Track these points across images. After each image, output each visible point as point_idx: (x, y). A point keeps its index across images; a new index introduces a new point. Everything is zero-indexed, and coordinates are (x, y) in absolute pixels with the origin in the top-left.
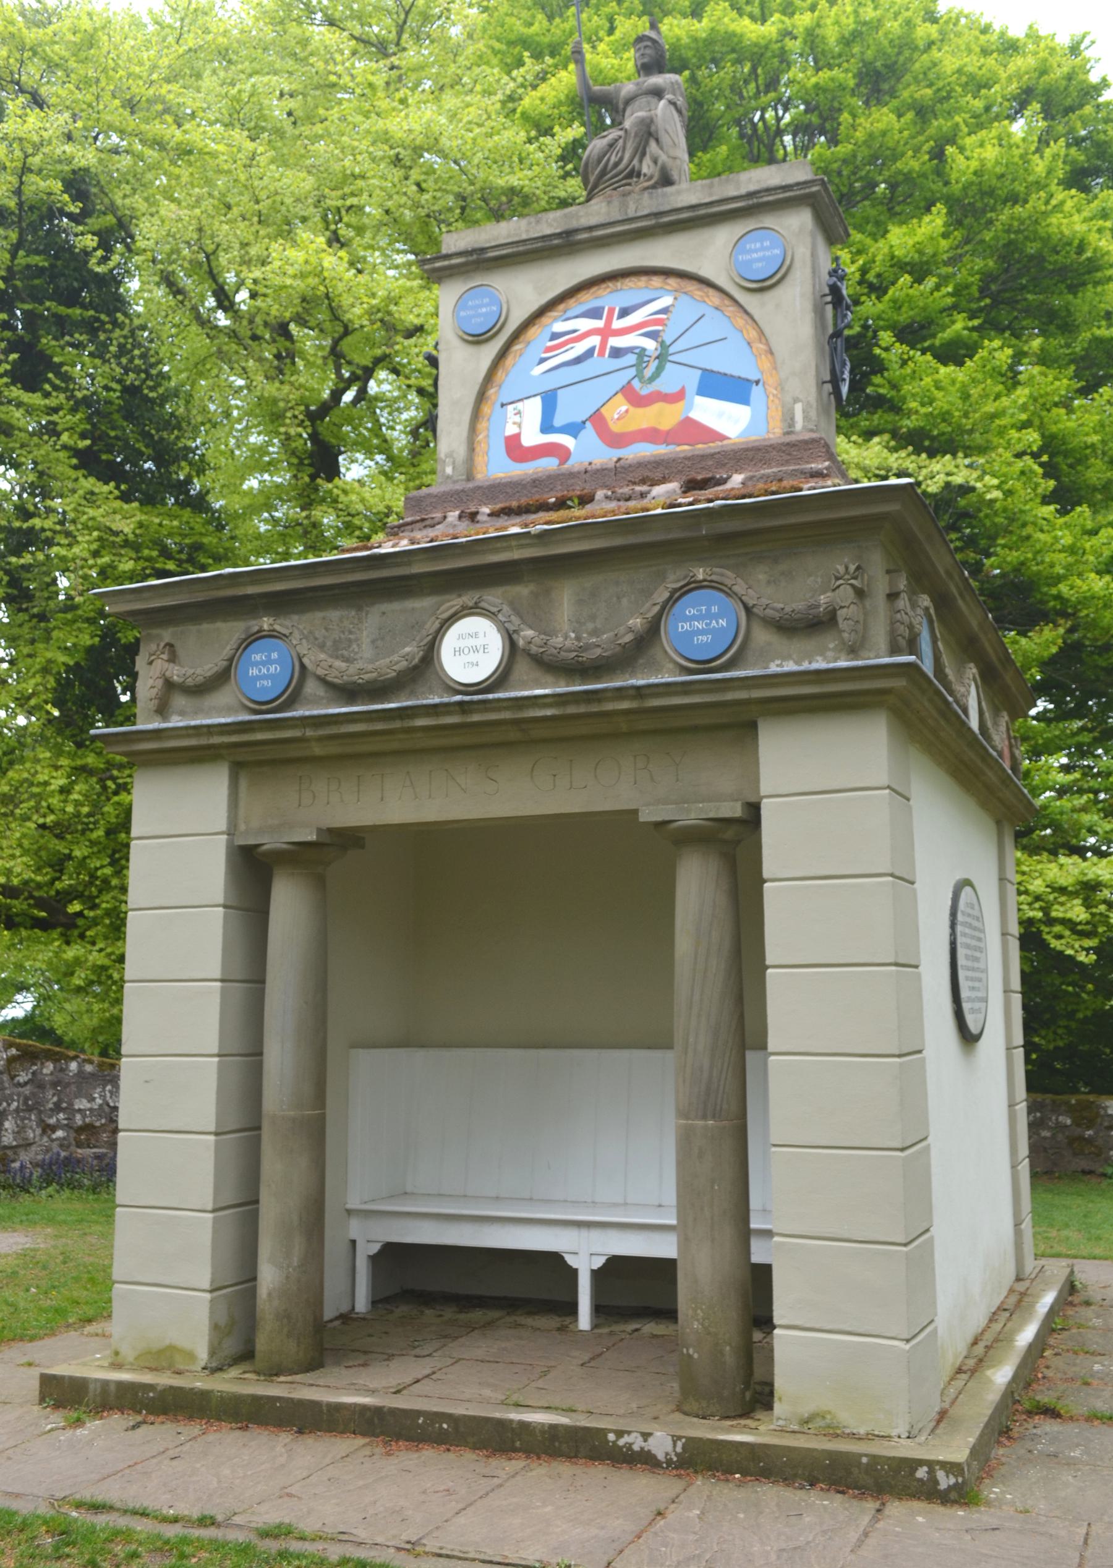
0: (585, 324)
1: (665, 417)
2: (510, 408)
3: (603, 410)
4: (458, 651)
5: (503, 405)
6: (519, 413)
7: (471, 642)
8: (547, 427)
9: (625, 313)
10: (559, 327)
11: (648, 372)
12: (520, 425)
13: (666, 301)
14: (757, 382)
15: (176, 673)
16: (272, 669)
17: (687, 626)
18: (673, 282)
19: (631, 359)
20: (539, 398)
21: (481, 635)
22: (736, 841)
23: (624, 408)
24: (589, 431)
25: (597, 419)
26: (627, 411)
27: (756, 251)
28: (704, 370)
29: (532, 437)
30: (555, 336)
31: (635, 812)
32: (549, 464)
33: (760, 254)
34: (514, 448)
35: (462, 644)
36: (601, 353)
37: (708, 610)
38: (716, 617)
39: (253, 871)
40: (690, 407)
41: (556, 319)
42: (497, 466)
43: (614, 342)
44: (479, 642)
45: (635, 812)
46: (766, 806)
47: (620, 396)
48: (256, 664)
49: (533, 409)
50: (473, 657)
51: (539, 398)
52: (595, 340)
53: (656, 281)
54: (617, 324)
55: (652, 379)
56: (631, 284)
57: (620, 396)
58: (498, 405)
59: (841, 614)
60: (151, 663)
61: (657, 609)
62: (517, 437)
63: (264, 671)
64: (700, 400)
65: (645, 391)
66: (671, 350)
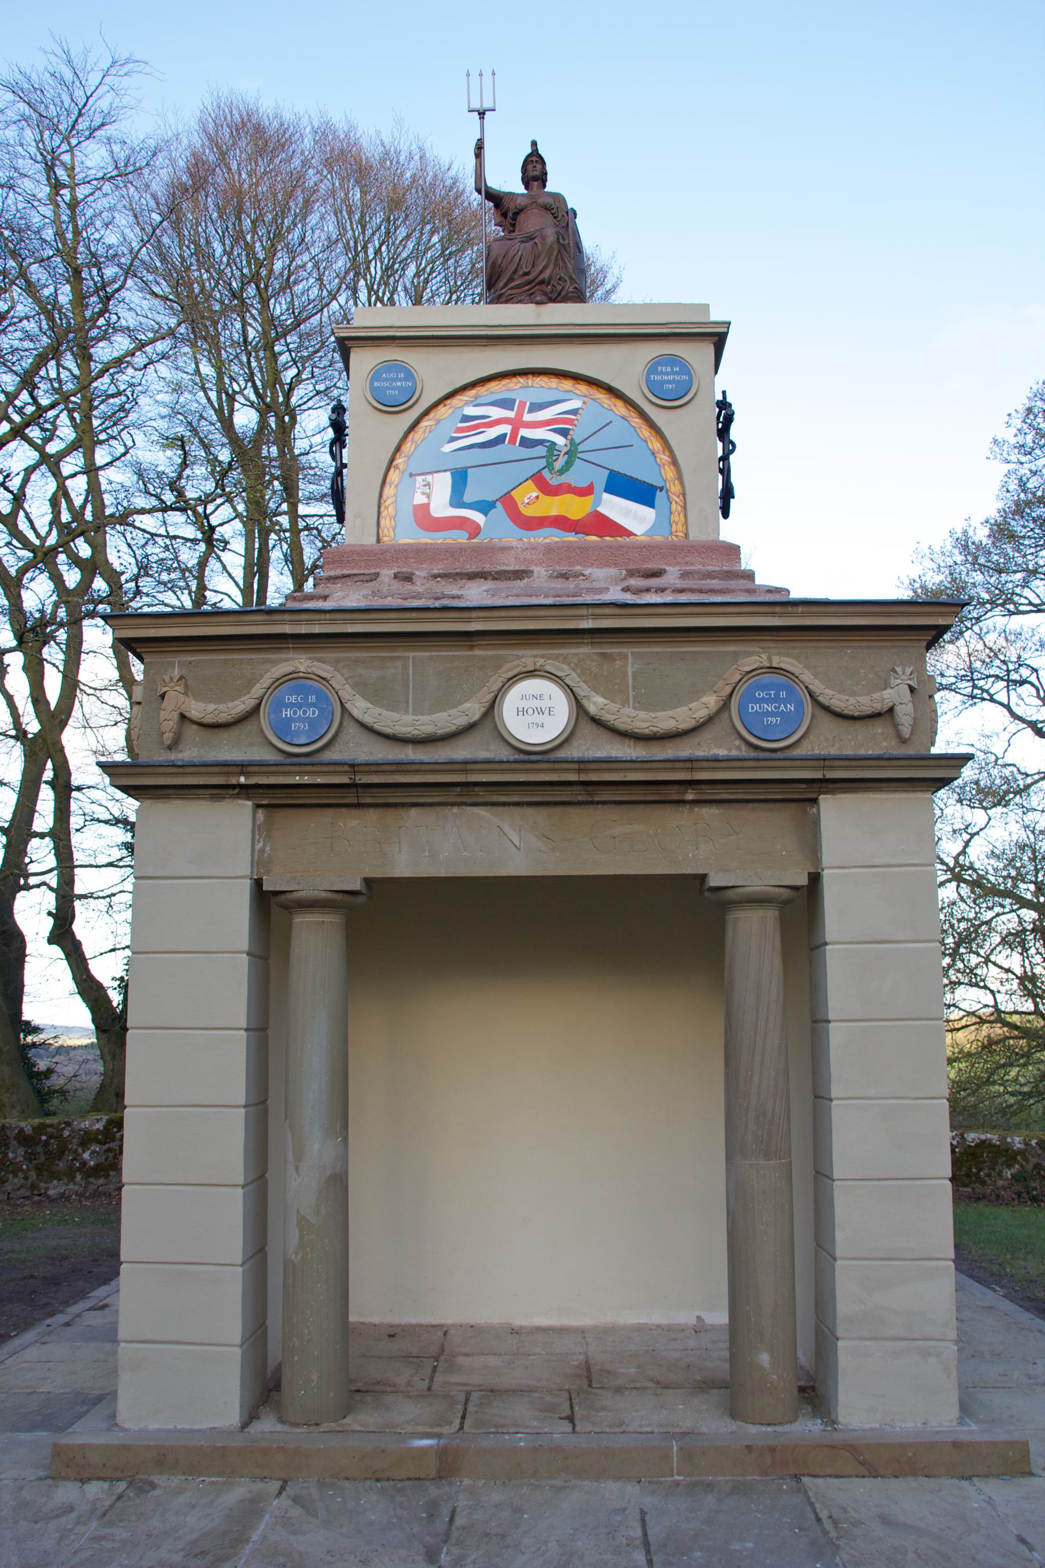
0: (496, 413)
1: (575, 508)
2: (419, 479)
3: (513, 493)
4: (522, 712)
5: (411, 475)
6: (428, 485)
7: (537, 704)
8: (457, 499)
9: (535, 407)
10: (470, 411)
11: (558, 465)
12: (429, 496)
13: (575, 404)
14: (661, 489)
15: (197, 709)
16: (310, 713)
17: (756, 707)
18: (583, 388)
19: (541, 450)
20: (448, 474)
21: (546, 697)
22: (801, 909)
23: (535, 495)
24: (499, 510)
25: (508, 501)
26: (537, 497)
27: (667, 374)
28: (612, 471)
29: (441, 507)
30: (466, 419)
31: (703, 877)
32: (460, 537)
33: (671, 378)
34: (423, 516)
35: (525, 704)
36: (513, 440)
37: (777, 695)
38: (785, 702)
39: (270, 907)
40: (599, 502)
41: (467, 403)
42: (405, 533)
43: (524, 432)
44: (544, 704)
45: (703, 877)
46: (826, 873)
47: (530, 482)
48: (291, 705)
49: (443, 483)
50: (537, 718)
51: (448, 474)
52: (506, 429)
53: (567, 384)
54: (527, 417)
55: (561, 472)
56: (543, 384)
57: (530, 482)
58: (407, 474)
59: (899, 710)
60: (163, 696)
61: (729, 689)
62: (426, 507)
63: (300, 713)
64: (606, 496)
65: (554, 481)
66: (581, 448)
